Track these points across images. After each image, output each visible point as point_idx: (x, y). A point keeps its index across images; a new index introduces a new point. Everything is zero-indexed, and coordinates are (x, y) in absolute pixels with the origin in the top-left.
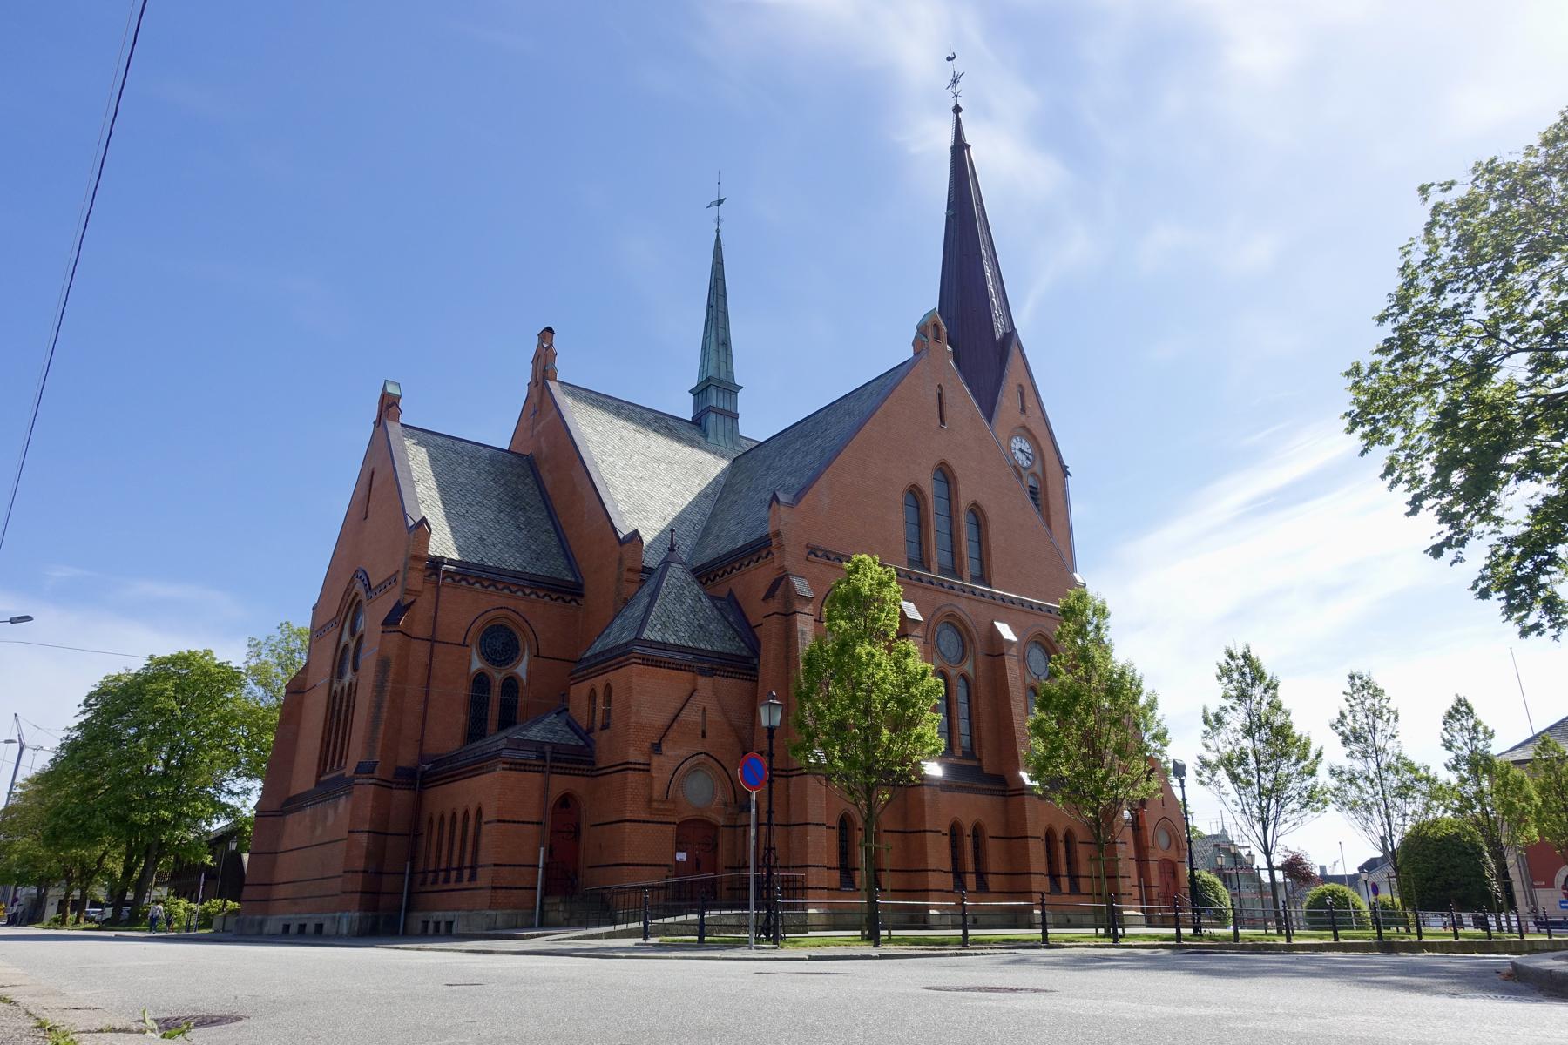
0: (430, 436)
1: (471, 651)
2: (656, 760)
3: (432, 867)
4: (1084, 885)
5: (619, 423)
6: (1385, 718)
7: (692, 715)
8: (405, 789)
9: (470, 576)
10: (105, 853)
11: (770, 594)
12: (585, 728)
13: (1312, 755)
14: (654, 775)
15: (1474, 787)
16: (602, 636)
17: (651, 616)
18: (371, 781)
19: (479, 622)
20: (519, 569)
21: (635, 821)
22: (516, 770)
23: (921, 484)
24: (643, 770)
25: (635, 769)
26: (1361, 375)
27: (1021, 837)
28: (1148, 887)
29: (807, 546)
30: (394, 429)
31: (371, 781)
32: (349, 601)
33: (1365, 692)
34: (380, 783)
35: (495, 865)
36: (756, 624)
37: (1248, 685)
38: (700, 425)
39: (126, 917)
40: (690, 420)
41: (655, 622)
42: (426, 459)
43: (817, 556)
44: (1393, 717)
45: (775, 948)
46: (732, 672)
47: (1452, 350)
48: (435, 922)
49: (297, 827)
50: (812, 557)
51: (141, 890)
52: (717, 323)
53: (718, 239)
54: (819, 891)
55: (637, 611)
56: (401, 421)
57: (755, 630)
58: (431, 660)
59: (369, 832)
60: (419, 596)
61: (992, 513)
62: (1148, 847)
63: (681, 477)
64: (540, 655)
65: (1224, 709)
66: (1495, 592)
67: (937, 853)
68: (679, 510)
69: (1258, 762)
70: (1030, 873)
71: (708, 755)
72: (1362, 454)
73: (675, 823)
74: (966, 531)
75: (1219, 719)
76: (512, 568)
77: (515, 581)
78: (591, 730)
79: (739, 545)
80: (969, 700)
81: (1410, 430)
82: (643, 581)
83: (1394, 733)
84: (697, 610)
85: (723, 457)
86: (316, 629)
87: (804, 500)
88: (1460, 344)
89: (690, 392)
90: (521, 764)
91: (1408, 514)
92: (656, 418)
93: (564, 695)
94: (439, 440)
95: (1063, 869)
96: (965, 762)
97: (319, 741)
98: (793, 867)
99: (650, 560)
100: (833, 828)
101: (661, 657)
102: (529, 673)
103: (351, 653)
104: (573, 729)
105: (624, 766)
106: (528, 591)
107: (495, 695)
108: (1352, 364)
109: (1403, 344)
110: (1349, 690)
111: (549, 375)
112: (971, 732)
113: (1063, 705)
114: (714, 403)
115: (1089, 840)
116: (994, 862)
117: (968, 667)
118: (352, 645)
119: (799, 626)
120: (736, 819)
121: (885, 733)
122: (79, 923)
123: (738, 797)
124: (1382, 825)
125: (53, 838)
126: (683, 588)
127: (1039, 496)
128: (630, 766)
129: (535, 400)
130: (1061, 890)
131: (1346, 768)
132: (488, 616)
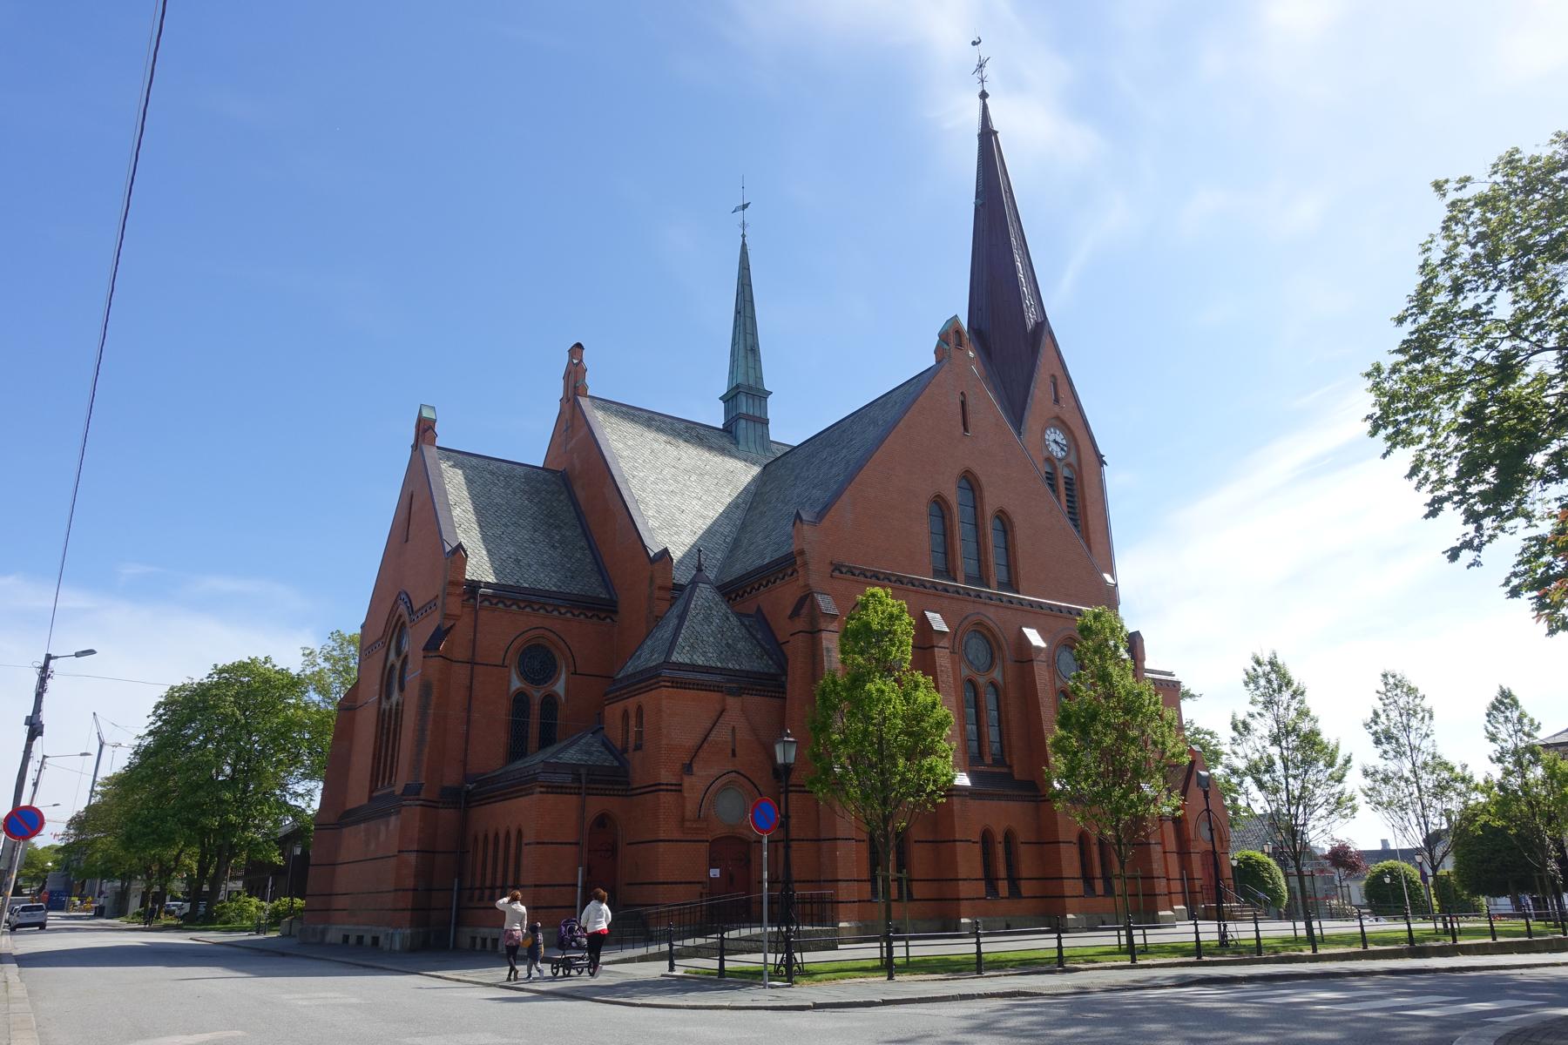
1: (509, 672)
2: (687, 781)
3: (478, 884)
5: (650, 435)
6: (1419, 716)
7: (721, 735)
10: (181, 851)
11: (795, 613)
12: (619, 748)
13: (1340, 761)
14: (686, 795)
15: (1519, 780)
16: (634, 657)
17: (680, 639)
18: (418, 803)
19: (516, 643)
20: (554, 589)
21: (669, 841)
22: (552, 793)
23: (945, 494)
24: (676, 791)
25: (667, 790)
26: (1382, 376)
28: (1191, 879)
30: (430, 453)
31: (418, 803)
32: (394, 621)
33: (1399, 691)
35: (536, 886)
36: (784, 641)
37: (1274, 691)
38: (731, 432)
39: (202, 913)
40: (721, 427)
41: (683, 644)
42: (463, 481)
43: (841, 573)
44: (1427, 715)
45: (789, 986)
46: (760, 691)
47: (1475, 350)
48: (482, 939)
49: (354, 841)
50: (836, 574)
51: (215, 883)
52: (745, 329)
53: (744, 245)
54: (849, 905)
55: (665, 633)
56: (437, 444)
57: (783, 646)
58: (471, 683)
59: (417, 851)
61: (1018, 520)
63: (712, 488)
65: (1251, 716)
66: (1526, 592)
67: (968, 862)
68: (709, 522)
69: (1286, 768)
70: (1062, 878)
71: (739, 773)
72: (1384, 456)
73: (707, 841)
75: (1246, 726)
76: (547, 588)
77: (551, 601)
78: (625, 750)
79: (767, 561)
80: (998, 707)
81: (1436, 430)
82: (674, 599)
83: (1429, 732)
84: (725, 630)
85: (754, 464)
86: (365, 648)
87: (827, 517)
88: (1483, 344)
89: (720, 399)
90: (558, 787)
91: (1426, 517)
92: (687, 428)
93: (599, 714)
94: (474, 461)
95: (1098, 872)
96: (996, 770)
97: (371, 756)
98: (824, 881)
99: (682, 577)
100: (864, 841)
101: (689, 679)
102: (567, 691)
103: (397, 673)
104: (607, 748)
105: (656, 788)
106: (563, 611)
107: (536, 709)
108: (1373, 365)
109: (1421, 345)
110: (1382, 689)
111: (580, 391)
112: (1000, 739)
113: (1082, 723)
114: (743, 410)
116: (1027, 866)
117: (997, 675)
118: (398, 666)
119: (825, 643)
121: (901, 762)
122: (160, 918)
124: (1419, 824)
125: (128, 841)
127: (1075, 487)
128: (662, 787)
129: (567, 416)
131: (1380, 768)
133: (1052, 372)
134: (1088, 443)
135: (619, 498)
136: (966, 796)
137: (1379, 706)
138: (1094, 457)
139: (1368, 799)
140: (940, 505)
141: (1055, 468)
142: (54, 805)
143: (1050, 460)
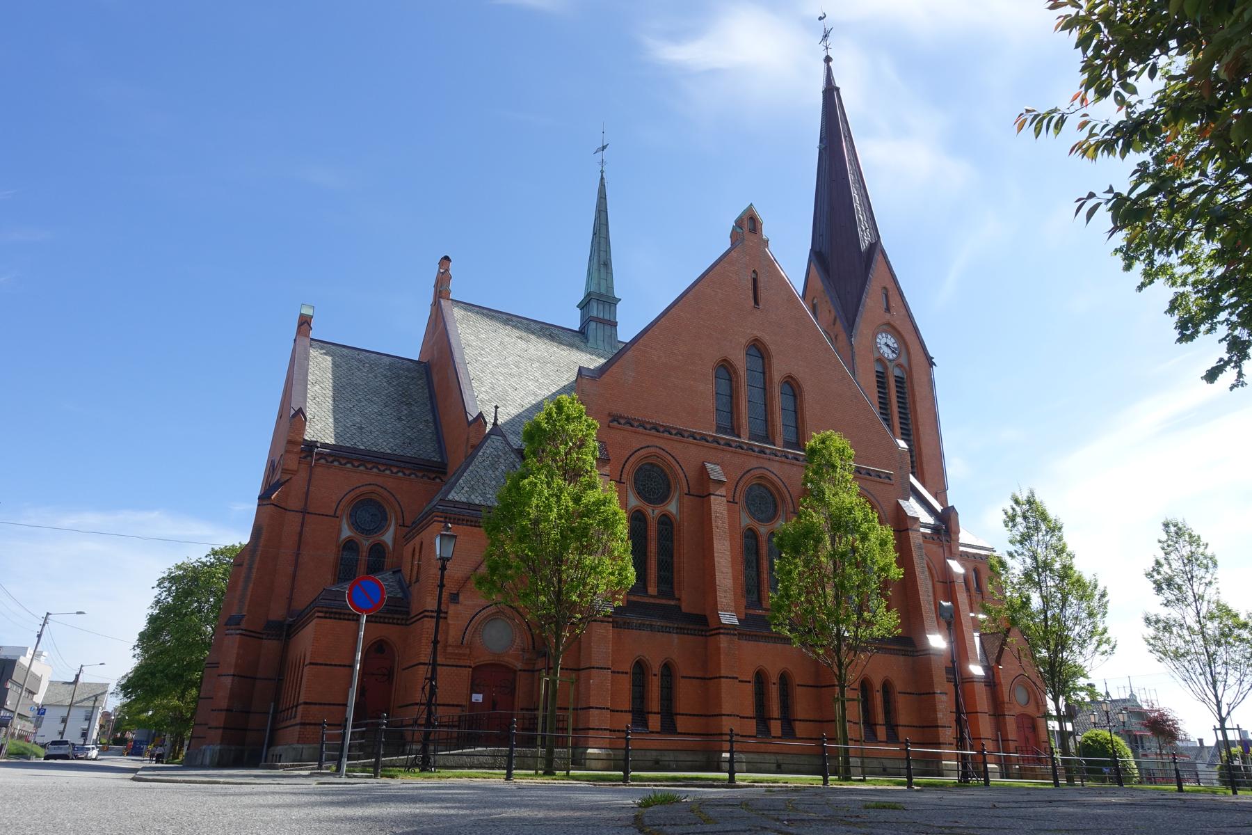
0: (338, 348)
4: (800, 728)
8: (274, 639)
9: (341, 457)
14: (450, 622)
18: (238, 632)
20: (389, 451)
23: (732, 358)
27: (830, 686)
29: (609, 415)
31: (238, 632)
34: (247, 633)
43: (619, 423)
53: (602, 178)
58: (302, 530)
60: (295, 475)
62: (1004, 703)
64: (406, 525)
73: (470, 667)
74: (779, 400)
76: (382, 450)
92: (542, 328)
94: (346, 351)
100: (626, 673)
102: (395, 540)
115: (909, 691)
116: (904, 715)
120: (534, 664)
123: (536, 644)
124: (1204, 673)
126: (499, 457)
127: (905, 385)
130: (898, 739)
131: (1162, 617)
132: (358, 492)
133: (884, 285)
134: (918, 347)
136: (735, 635)
137: (1161, 555)
138: (923, 359)
139: (1151, 648)
140: (725, 368)
141: (886, 367)
142: (101, 664)
143: (881, 360)
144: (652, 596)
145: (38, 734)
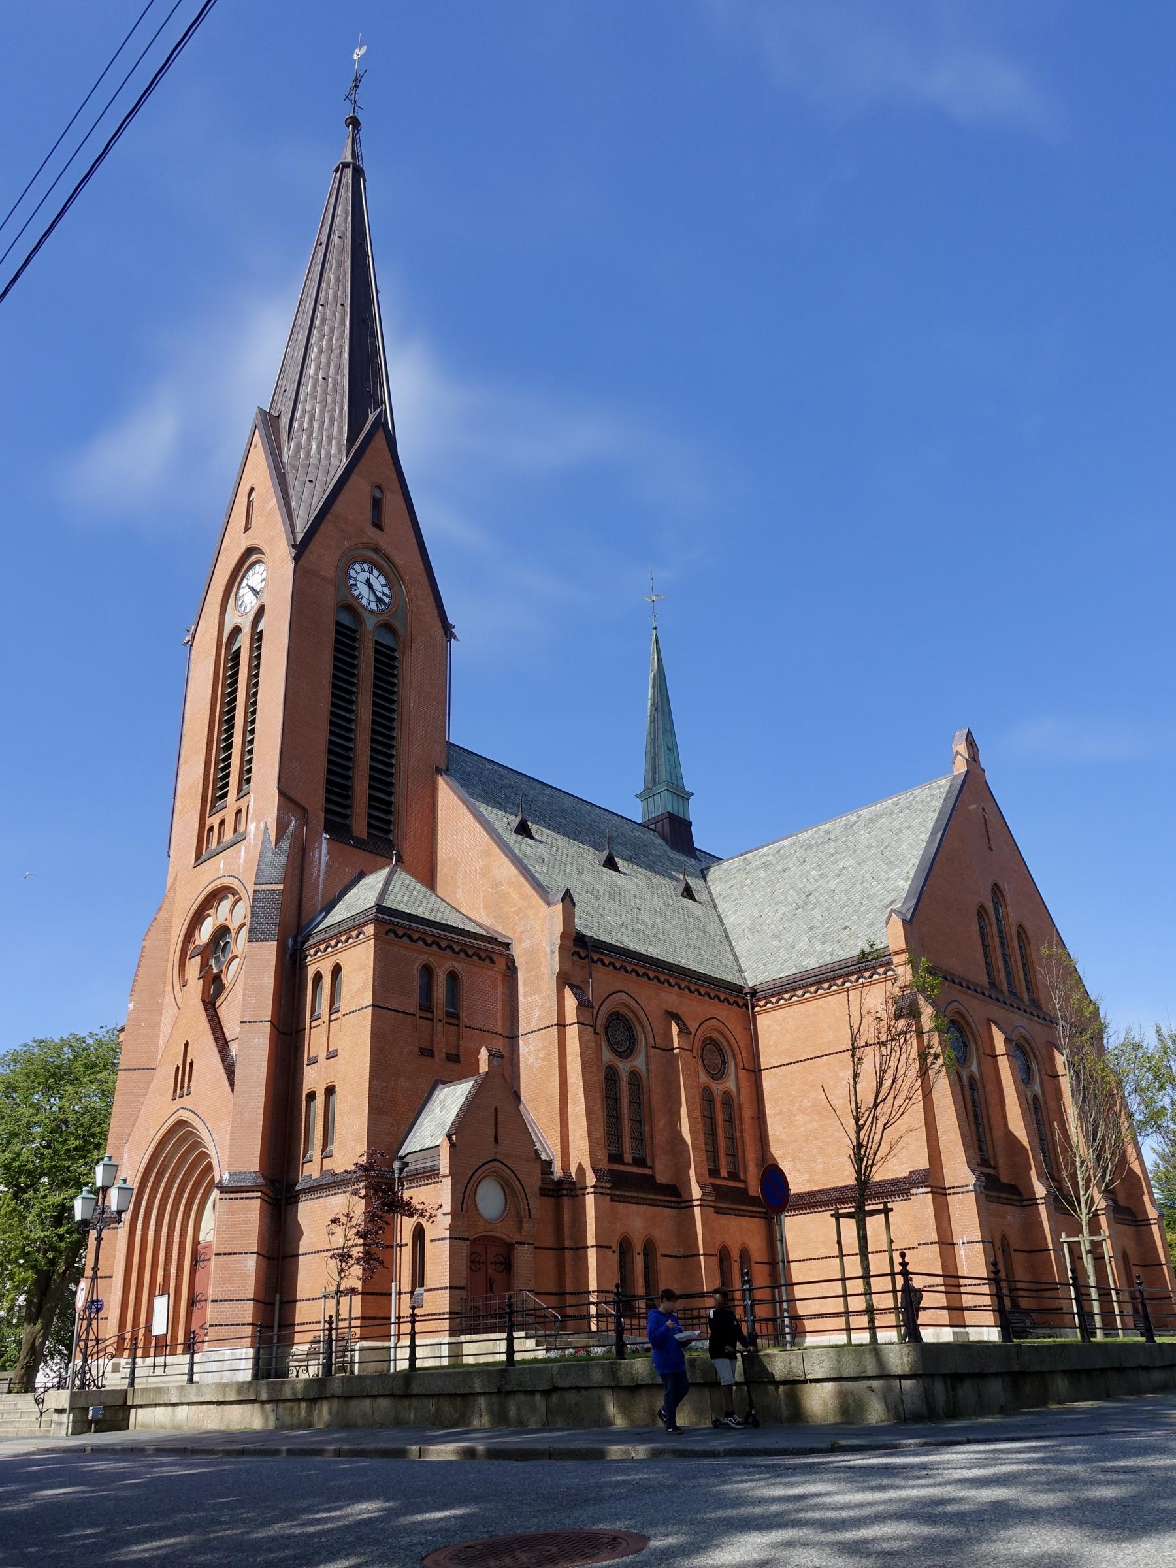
73: (468, 1239)
135: (988, 793)
144: (724, 1178)
145: (100, 1317)
